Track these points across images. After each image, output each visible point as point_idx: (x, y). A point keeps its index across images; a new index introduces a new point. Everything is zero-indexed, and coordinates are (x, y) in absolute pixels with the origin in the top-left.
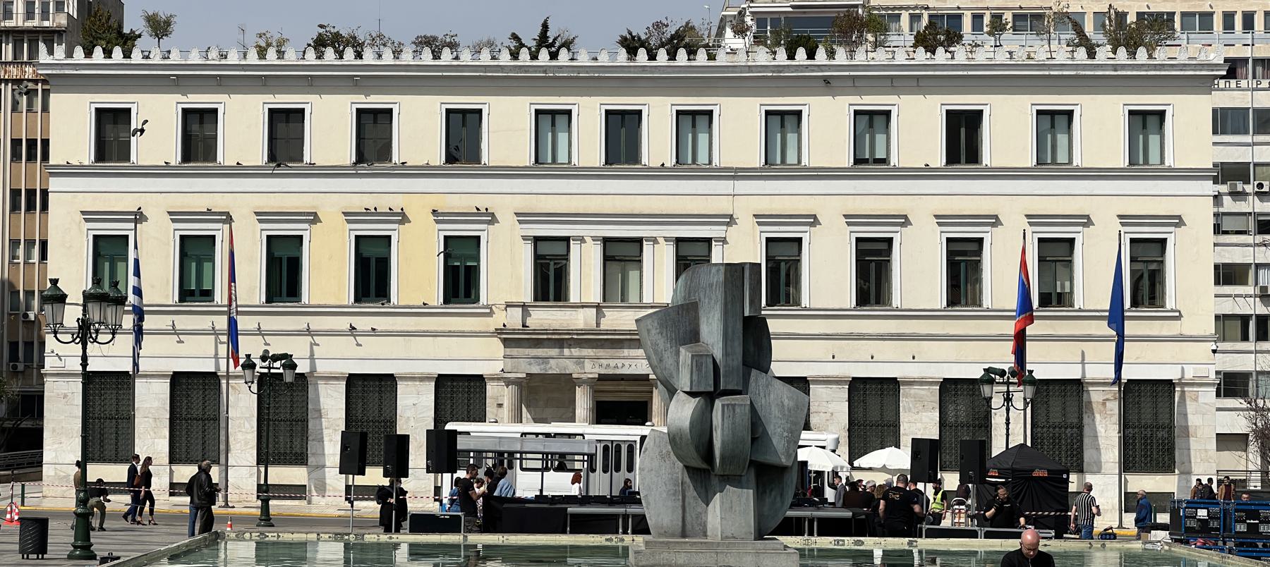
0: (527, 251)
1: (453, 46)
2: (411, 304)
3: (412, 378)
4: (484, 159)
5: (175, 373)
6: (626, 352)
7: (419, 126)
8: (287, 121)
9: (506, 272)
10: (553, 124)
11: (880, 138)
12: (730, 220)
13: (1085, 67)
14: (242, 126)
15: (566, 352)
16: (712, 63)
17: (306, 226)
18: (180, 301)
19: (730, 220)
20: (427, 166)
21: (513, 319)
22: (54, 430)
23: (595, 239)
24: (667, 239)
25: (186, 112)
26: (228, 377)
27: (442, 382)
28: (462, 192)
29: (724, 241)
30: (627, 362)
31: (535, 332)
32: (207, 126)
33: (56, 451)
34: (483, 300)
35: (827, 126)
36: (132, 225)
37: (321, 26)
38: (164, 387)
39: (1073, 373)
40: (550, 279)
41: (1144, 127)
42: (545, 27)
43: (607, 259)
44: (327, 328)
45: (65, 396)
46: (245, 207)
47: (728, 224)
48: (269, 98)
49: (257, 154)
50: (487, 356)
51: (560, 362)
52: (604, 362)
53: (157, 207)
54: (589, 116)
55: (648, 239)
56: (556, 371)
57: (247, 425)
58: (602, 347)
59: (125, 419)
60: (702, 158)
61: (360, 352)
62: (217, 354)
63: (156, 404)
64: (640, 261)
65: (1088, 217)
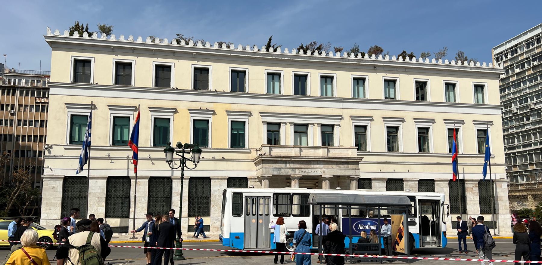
0: (264, 128)
1: (319, 49)
2: (217, 148)
3: (218, 178)
6: (312, 166)
7: (220, 75)
8: (163, 70)
9: (256, 135)
11: (392, 90)
13: (346, 60)
14: (143, 70)
15: (288, 166)
16: (228, 49)
17: (171, 114)
19: (341, 118)
20: (224, 92)
22: (47, 204)
23: (290, 123)
24: (318, 124)
25: (157, 66)
26: (136, 178)
27: (110, 180)
28: (238, 103)
29: (339, 125)
30: (313, 170)
31: (276, 157)
32: (127, 70)
33: (47, 213)
34: (247, 146)
35: (375, 83)
36: (90, 111)
37: (178, 35)
38: (146, 182)
39: (125, 174)
40: (273, 139)
41: (326, 82)
42: (270, 39)
43: (295, 132)
44: (232, 158)
45: (54, 188)
47: (341, 119)
48: (155, 59)
49: (150, 83)
50: (430, 172)
51: (286, 170)
52: (304, 170)
53: (104, 105)
54: (288, 76)
55: (311, 124)
56: (284, 174)
57: (143, 200)
58: (303, 164)
59: (84, 198)
60: (277, 92)
61: (153, 167)
62: (128, 168)
63: (99, 191)
65: (214, 111)
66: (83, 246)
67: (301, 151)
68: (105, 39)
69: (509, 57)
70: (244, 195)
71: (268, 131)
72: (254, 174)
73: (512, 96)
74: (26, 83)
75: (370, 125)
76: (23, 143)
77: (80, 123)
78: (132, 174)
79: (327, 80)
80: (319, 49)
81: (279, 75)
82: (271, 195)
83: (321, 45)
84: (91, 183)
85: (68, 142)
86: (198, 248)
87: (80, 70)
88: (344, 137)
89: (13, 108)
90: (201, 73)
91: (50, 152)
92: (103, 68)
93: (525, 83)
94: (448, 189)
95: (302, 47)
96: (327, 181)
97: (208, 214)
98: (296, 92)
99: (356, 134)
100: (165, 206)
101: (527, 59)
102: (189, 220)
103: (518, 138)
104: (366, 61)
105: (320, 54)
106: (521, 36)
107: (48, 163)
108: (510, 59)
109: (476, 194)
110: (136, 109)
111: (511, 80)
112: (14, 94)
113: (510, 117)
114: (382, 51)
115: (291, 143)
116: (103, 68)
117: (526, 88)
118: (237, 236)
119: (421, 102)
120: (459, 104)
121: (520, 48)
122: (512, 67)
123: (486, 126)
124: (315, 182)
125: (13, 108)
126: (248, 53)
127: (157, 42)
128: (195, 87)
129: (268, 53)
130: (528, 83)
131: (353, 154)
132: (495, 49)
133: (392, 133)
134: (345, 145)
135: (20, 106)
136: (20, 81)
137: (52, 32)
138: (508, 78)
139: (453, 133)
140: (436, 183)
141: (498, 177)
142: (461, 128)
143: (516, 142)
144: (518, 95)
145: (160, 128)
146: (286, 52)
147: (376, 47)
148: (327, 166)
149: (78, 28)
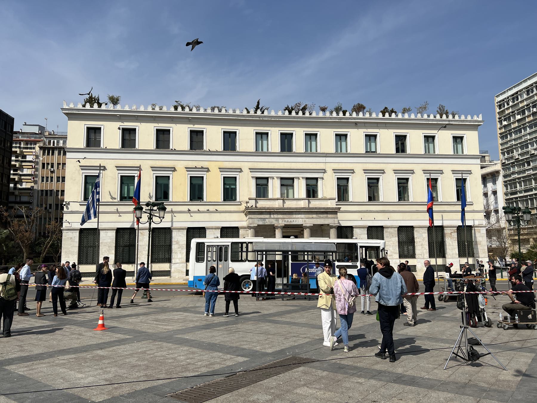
0: (253, 183)
3: (212, 228)
4: (238, 149)
5: (118, 228)
6: (294, 216)
7: (213, 137)
8: (164, 134)
9: (246, 189)
10: (262, 138)
11: (373, 144)
12: (324, 171)
14: (146, 135)
15: (272, 216)
16: (220, 113)
17: (171, 172)
18: (121, 200)
19: (324, 171)
20: (217, 151)
21: (252, 203)
22: (66, 252)
23: (277, 178)
24: (303, 178)
27: (119, 231)
29: (323, 178)
30: (295, 220)
31: (260, 209)
34: (238, 199)
35: (356, 139)
36: (98, 171)
37: (176, 102)
42: (258, 103)
43: (282, 185)
44: (225, 210)
45: (71, 238)
46: (147, 167)
47: (324, 173)
48: (156, 125)
51: (270, 220)
52: (286, 220)
54: (275, 135)
55: (296, 178)
56: (269, 223)
58: (285, 214)
59: (96, 247)
63: (109, 241)
64: (293, 186)
65: (208, 168)
66: (4, 283)
67: (284, 203)
68: (112, 109)
69: (511, 104)
70: (206, 244)
71: (257, 185)
72: (245, 224)
73: (513, 142)
74: (63, 143)
75: (351, 177)
76: (62, 197)
77: (91, 184)
78: (136, 226)
79: (311, 137)
80: (304, 109)
81: (267, 134)
82: (230, 244)
83: (306, 105)
84: (175, 234)
85: (83, 199)
86: (181, 289)
87: (92, 136)
88: (328, 189)
89: (52, 167)
90: (197, 135)
91: (68, 208)
92: (111, 135)
93: (525, 129)
94: (427, 234)
95: (287, 109)
96: (308, 229)
97: (413, 256)
98: (283, 149)
99: (338, 185)
100: (166, 254)
101: (527, 105)
102: (187, 265)
103: (520, 183)
104: (347, 118)
105: (304, 114)
106: (521, 83)
107: (66, 217)
108: (512, 106)
109: (455, 239)
110: (139, 169)
111: (513, 126)
112: (53, 154)
113: (513, 163)
114: (364, 108)
115: (278, 195)
116: (111, 135)
117: (527, 134)
118: (200, 279)
119: (400, 154)
120: (438, 155)
121: (520, 95)
122: (513, 114)
123: (461, 175)
124: (295, 231)
125: (52, 167)
126: (238, 116)
127: (157, 109)
128: (191, 148)
129: (256, 115)
130: (528, 129)
131: (332, 204)
132: (497, 96)
133: (373, 185)
134: (328, 197)
135: (59, 164)
136: (58, 142)
137: (68, 105)
138: (509, 125)
139: (432, 183)
140: (415, 229)
141: (477, 223)
142: (440, 178)
143: (518, 188)
144: (519, 141)
145: (161, 185)
146: (273, 114)
147: (359, 104)
148: (307, 216)
149: (91, 100)
